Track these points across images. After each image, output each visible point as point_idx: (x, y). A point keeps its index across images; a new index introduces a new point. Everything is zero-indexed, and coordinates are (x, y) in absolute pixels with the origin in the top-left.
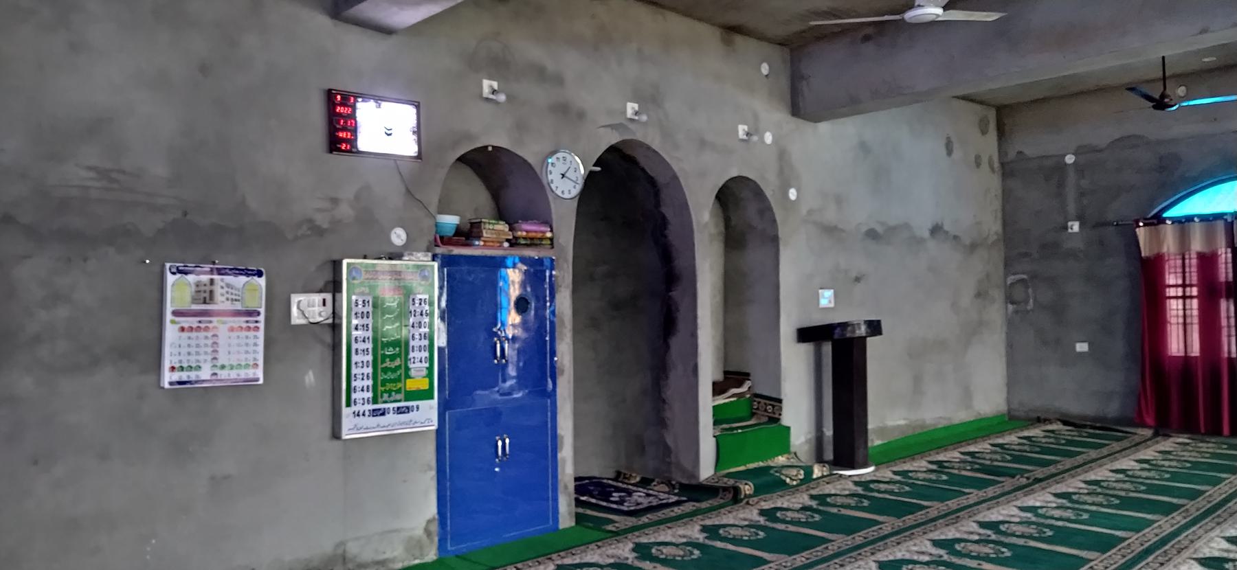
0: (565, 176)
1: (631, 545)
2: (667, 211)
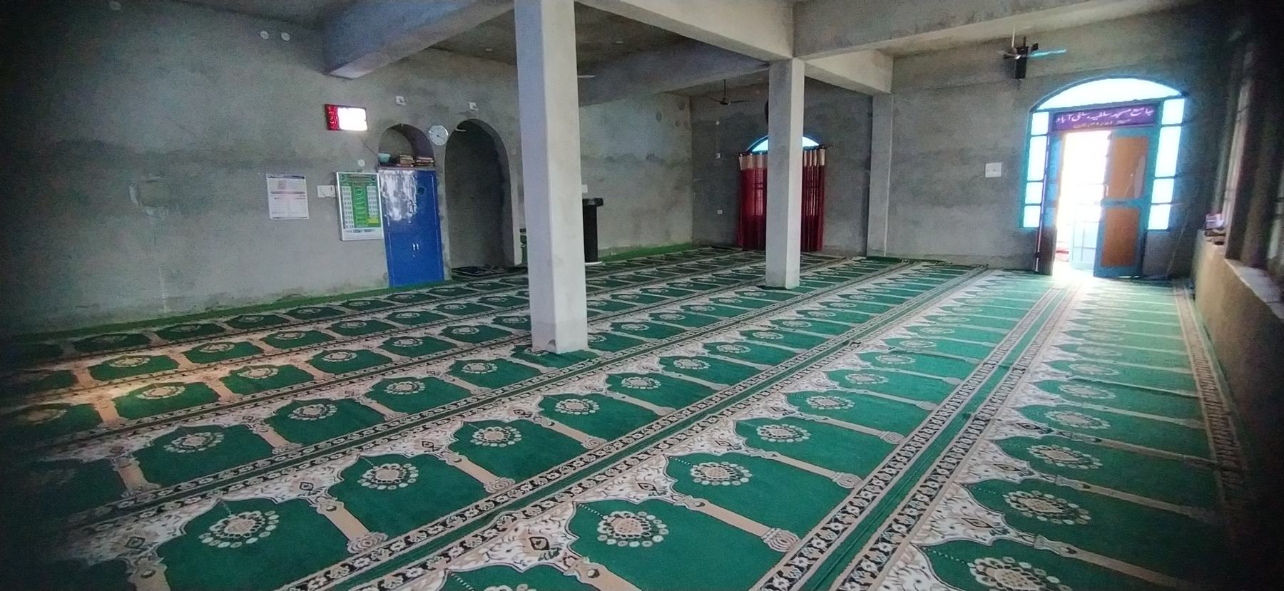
0: (439, 136)
1: (605, 377)
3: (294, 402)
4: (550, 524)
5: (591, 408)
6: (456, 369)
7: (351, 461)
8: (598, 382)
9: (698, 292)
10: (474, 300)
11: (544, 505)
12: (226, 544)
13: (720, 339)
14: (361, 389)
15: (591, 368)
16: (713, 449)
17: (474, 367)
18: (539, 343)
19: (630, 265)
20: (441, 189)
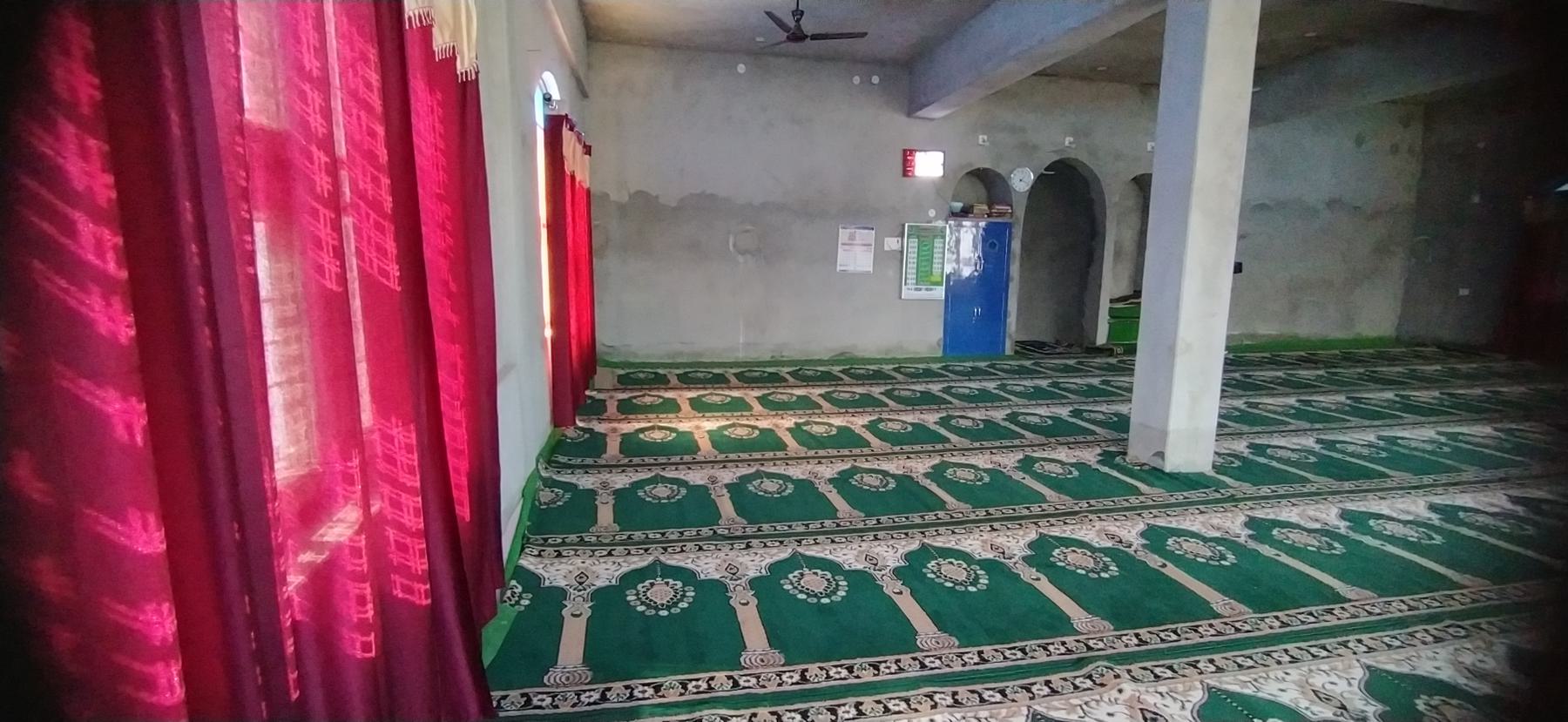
0: (1022, 180)
1: (1141, 527)
2: (1094, 195)
3: (854, 467)
4: (1168, 701)
5: (1106, 568)
6: (1027, 464)
7: (784, 554)
8: (1233, 523)
9: (1355, 421)
10: (1044, 383)
11: (986, 695)
12: (803, 596)
13: (1383, 508)
14: (920, 467)
15: (1217, 501)
16: (1304, 704)
17: (1049, 467)
18: (1138, 452)
19: (1275, 362)
20: (1016, 245)
